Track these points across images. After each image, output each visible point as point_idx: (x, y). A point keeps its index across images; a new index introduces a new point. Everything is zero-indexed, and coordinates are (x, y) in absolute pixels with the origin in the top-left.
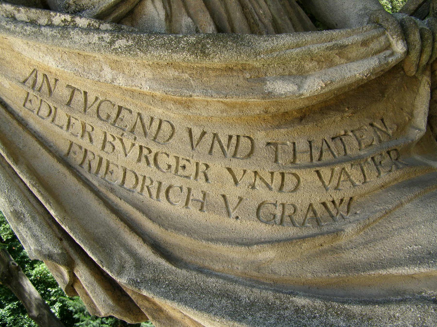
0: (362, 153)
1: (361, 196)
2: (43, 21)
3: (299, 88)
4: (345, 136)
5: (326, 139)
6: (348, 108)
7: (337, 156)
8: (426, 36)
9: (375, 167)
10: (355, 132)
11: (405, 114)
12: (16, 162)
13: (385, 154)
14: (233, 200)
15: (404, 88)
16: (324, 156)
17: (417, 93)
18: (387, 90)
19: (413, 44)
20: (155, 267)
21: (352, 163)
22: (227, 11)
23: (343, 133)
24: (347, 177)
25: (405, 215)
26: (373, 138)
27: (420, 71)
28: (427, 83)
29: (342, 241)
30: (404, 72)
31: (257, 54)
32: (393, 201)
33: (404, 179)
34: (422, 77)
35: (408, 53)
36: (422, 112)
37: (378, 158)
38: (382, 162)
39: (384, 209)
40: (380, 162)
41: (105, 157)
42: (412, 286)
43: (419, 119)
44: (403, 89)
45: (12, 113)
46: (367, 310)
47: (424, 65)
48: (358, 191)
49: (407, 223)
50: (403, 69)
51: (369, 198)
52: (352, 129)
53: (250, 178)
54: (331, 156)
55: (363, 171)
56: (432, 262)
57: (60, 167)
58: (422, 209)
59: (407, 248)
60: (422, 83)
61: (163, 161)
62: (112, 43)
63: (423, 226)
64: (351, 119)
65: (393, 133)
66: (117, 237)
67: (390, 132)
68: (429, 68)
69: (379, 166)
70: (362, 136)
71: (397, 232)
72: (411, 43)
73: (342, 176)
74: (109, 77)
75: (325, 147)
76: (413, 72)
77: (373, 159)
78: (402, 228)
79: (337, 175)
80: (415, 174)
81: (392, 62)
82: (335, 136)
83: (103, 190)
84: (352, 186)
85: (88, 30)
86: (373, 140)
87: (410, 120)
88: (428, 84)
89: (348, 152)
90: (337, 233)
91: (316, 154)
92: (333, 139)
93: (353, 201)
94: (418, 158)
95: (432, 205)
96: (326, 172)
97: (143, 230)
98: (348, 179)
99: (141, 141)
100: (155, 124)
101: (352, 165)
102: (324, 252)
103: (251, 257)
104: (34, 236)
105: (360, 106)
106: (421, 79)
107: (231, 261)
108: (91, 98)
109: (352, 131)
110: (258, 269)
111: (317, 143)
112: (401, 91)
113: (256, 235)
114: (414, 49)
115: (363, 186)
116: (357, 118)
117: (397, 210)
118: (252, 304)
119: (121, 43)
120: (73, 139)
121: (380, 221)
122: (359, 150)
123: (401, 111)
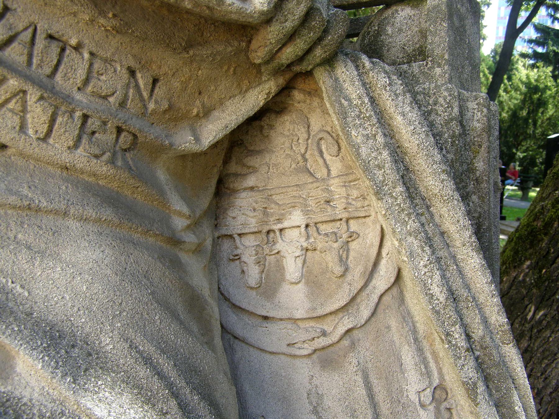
0: (78, 96)
1: (21, 154)
4: (74, 51)
5: (38, 28)
6: (115, 16)
7: (34, 66)
8: (313, 23)
9: (77, 132)
10: (96, 60)
11: (198, 103)
13: (111, 127)
15: (229, 68)
16: (12, 49)
17: (243, 92)
18: (200, 48)
19: (285, 16)
21: (45, 95)
23: (73, 42)
24: (20, 108)
25: (54, 233)
26: (116, 92)
27: (271, 66)
28: (267, 91)
30: (248, 46)
32: (57, 200)
33: (110, 186)
34: (268, 80)
36: (225, 122)
37: (93, 124)
38: (97, 135)
39: (32, 199)
40: (93, 133)
43: (211, 127)
44: (226, 68)
47: (282, 65)
48: (21, 143)
49: (43, 246)
50: (250, 42)
51: (32, 167)
52: (94, 50)
54: (24, 58)
55: (53, 121)
56: (16, 329)
58: (87, 245)
59: (4, 281)
60: (261, 86)
63: (59, 269)
64: (107, 36)
65: (154, 112)
67: (151, 106)
68: (288, 76)
69: (85, 136)
70: (102, 75)
71: (15, 246)
72: (284, 11)
73: (14, 101)
75: (26, 36)
76: (259, 57)
77: (85, 117)
78: (29, 248)
79: (7, 93)
80: (133, 193)
81: (230, 5)
82: (56, 35)
84: (18, 128)
86: (113, 94)
87: (197, 115)
88: (267, 94)
89: (59, 77)
92: (51, 37)
93: (4, 153)
94: (162, 175)
95: (106, 251)
98: (22, 114)
101: (41, 98)
105: (137, 30)
106: (265, 81)
109: (92, 54)
112: (222, 68)
114: (281, 23)
115: (35, 144)
116: (118, 42)
117: (51, 217)
121: (9, 212)
122: (79, 89)
123: (197, 94)
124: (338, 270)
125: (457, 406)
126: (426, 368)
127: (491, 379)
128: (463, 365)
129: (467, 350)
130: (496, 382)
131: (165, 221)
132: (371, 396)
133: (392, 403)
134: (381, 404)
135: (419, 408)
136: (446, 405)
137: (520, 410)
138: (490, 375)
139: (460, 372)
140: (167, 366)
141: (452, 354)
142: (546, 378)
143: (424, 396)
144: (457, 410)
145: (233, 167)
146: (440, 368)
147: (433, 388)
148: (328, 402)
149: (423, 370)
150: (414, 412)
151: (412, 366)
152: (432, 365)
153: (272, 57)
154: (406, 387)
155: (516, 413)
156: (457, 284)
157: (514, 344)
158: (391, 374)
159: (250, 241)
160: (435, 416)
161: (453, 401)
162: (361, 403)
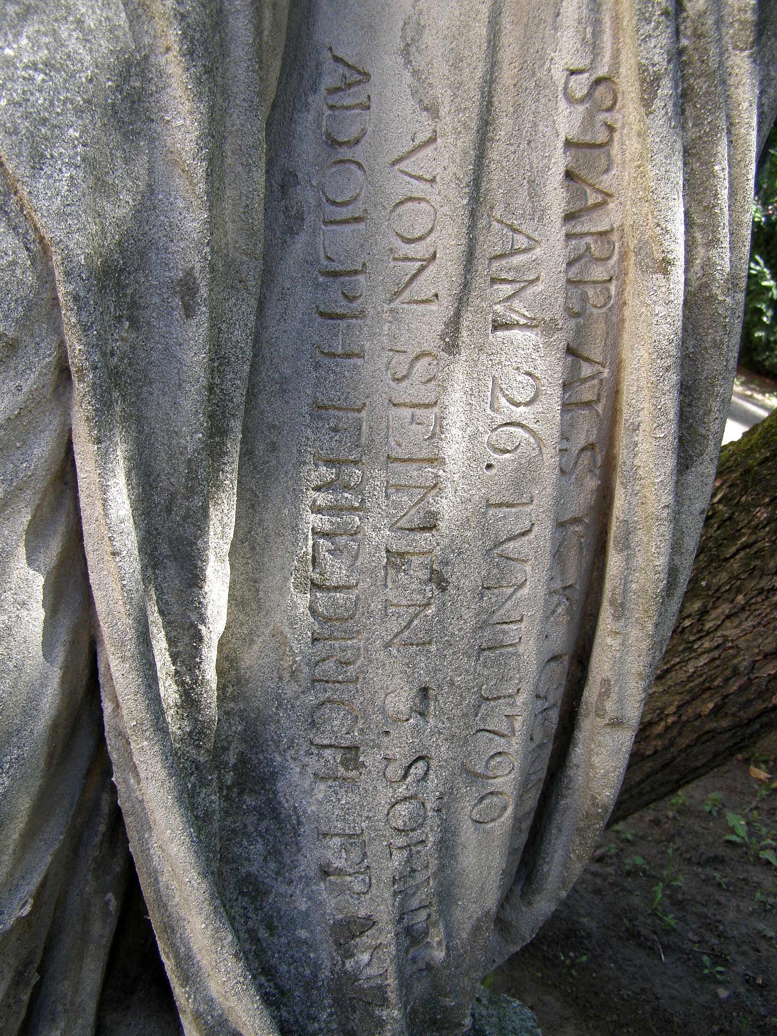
125: (623, 127)
126: (594, 34)
127: (692, 99)
128: (649, 36)
129: (666, 13)
130: (698, 106)
133: (521, 69)
134: (505, 66)
135: (561, 96)
136: (607, 118)
137: (721, 175)
138: (692, 90)
139: (640, 45)
141: (638, 7)
143: (575, 81)
144: (621, 134)
146: (618, 50)
147: (593, 78)
148: (428, 39)
149: (588, 36)
150: (550, 100)
151: (572, 22)
152: (607, 38)
154: (552, 54)
155: (714, 177)
157: (752, 54)
158: (536, 21)
160: (582, 123)
161: (621, 116)
162: (475, 49)
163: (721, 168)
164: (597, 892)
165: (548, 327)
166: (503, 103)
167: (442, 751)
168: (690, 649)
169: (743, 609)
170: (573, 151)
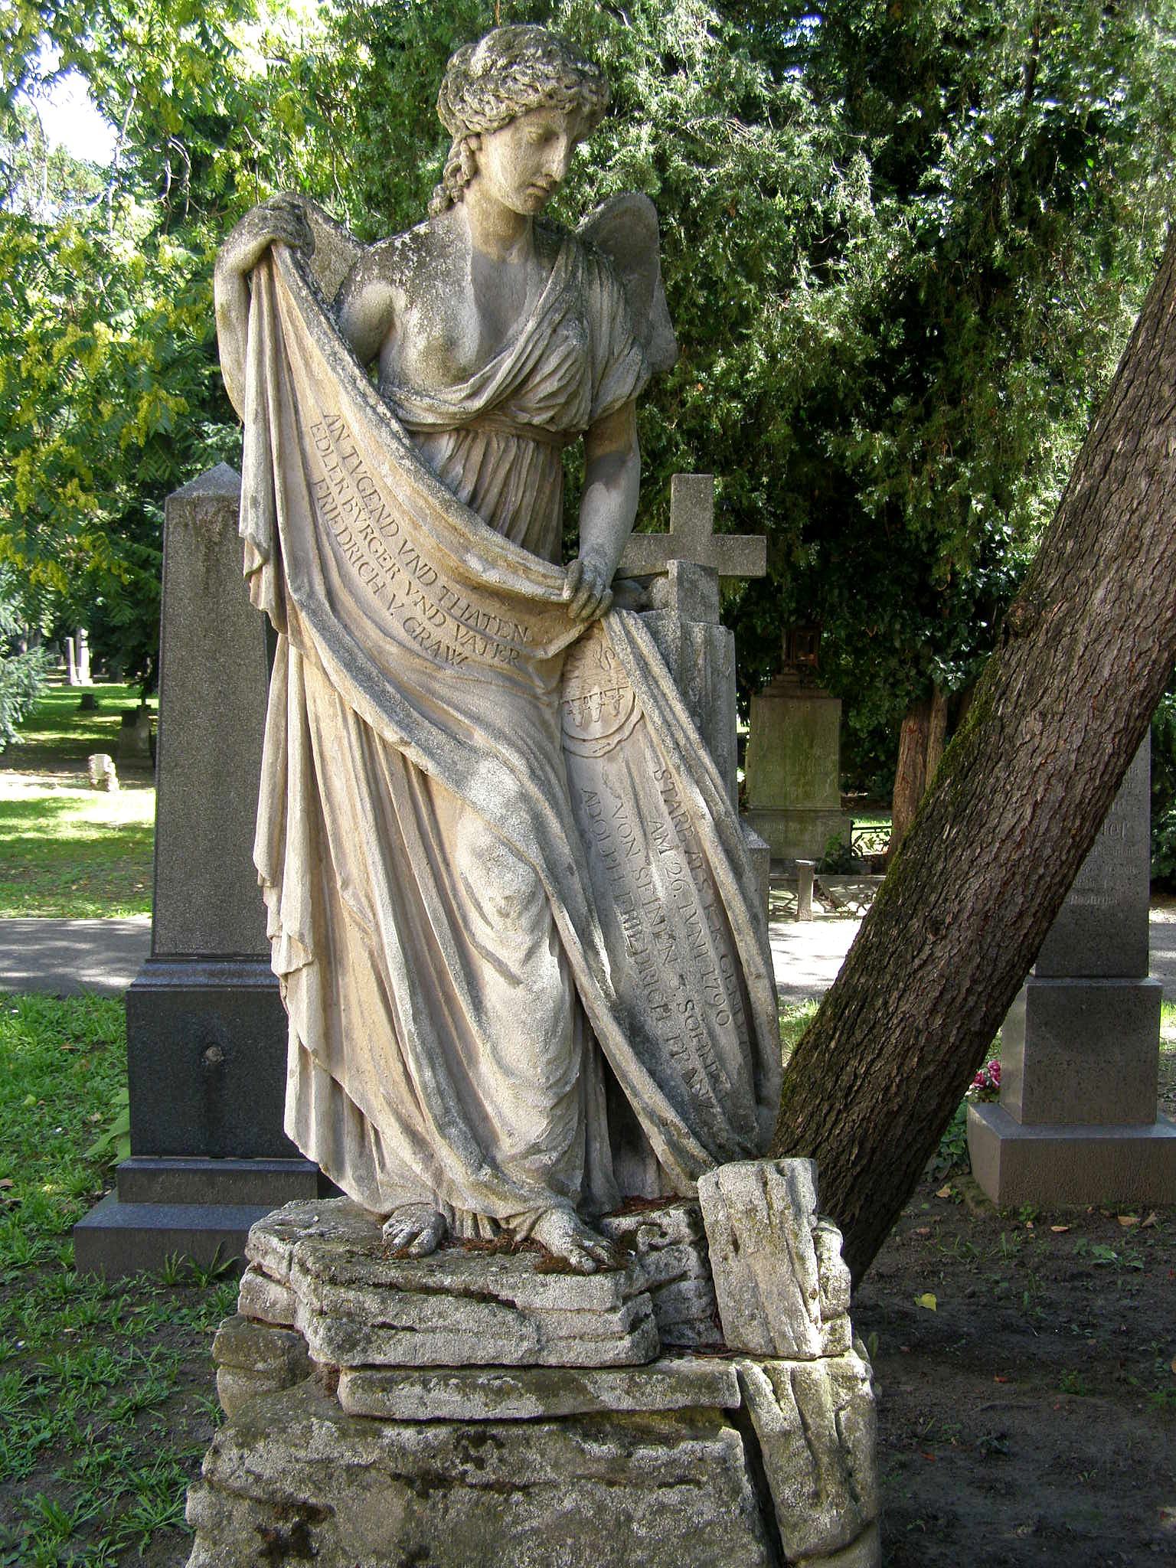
2: (372, 401)
3: (484, 571)
12: (279, 464)
14: (398, 602)
17: (568, 631)
20: (320, 605)
22: (490, 484)
29: (439, 675)
31: (475, 534)
35: (572, 601)
37: (501, 647)
41: (340, 509)
42: (455, 728)
45: (298, 421)
46: (420, 718)
53: (417, 597)
57: (305, 492)
61: (375, 545)
62: (402, 458)
66: (309, 566)
74: (384, 472)
83: (322, 529)
85: (395, 435)
90: (440, 668)
91: (467, 615)
94: (531, 669)
96: (463, 630)
97: (789, 675)
99: (372, 523)
100: (389, 520)
102: (425, 673)
103: (381, 643)
104: (257, 524)
107: (368, 637)
108: (362, 469)
110: (380, 653)
111: (473, 610)
113: (395, 633)
118: (362, 669)
119: (407, 463)
120: (328, 480)
124: (614, 713)
131: (532, 688)
132: (630, 774)
140: (530, 742)
142: (960, 902)
145: (569, 668)
153: (578, 615)
156: (670, 718)
159: (577, 703)
163: (709, 783)
164: (974, 1313)
165: (677, 847)
166: (639, 788)
167: (696, 997)
168: (887, 1029)
169: (905, 991)
170: (258, 951)
